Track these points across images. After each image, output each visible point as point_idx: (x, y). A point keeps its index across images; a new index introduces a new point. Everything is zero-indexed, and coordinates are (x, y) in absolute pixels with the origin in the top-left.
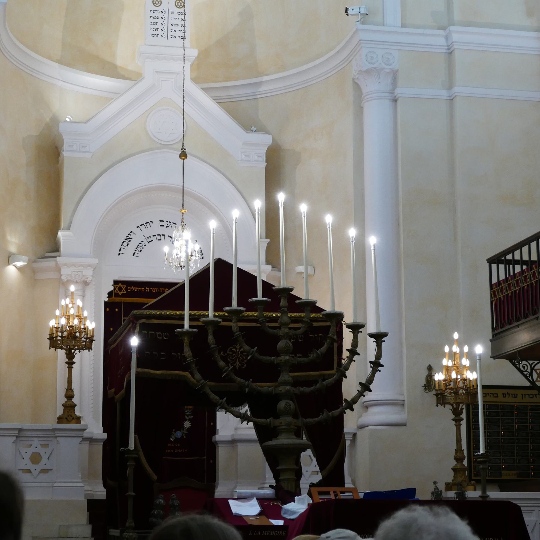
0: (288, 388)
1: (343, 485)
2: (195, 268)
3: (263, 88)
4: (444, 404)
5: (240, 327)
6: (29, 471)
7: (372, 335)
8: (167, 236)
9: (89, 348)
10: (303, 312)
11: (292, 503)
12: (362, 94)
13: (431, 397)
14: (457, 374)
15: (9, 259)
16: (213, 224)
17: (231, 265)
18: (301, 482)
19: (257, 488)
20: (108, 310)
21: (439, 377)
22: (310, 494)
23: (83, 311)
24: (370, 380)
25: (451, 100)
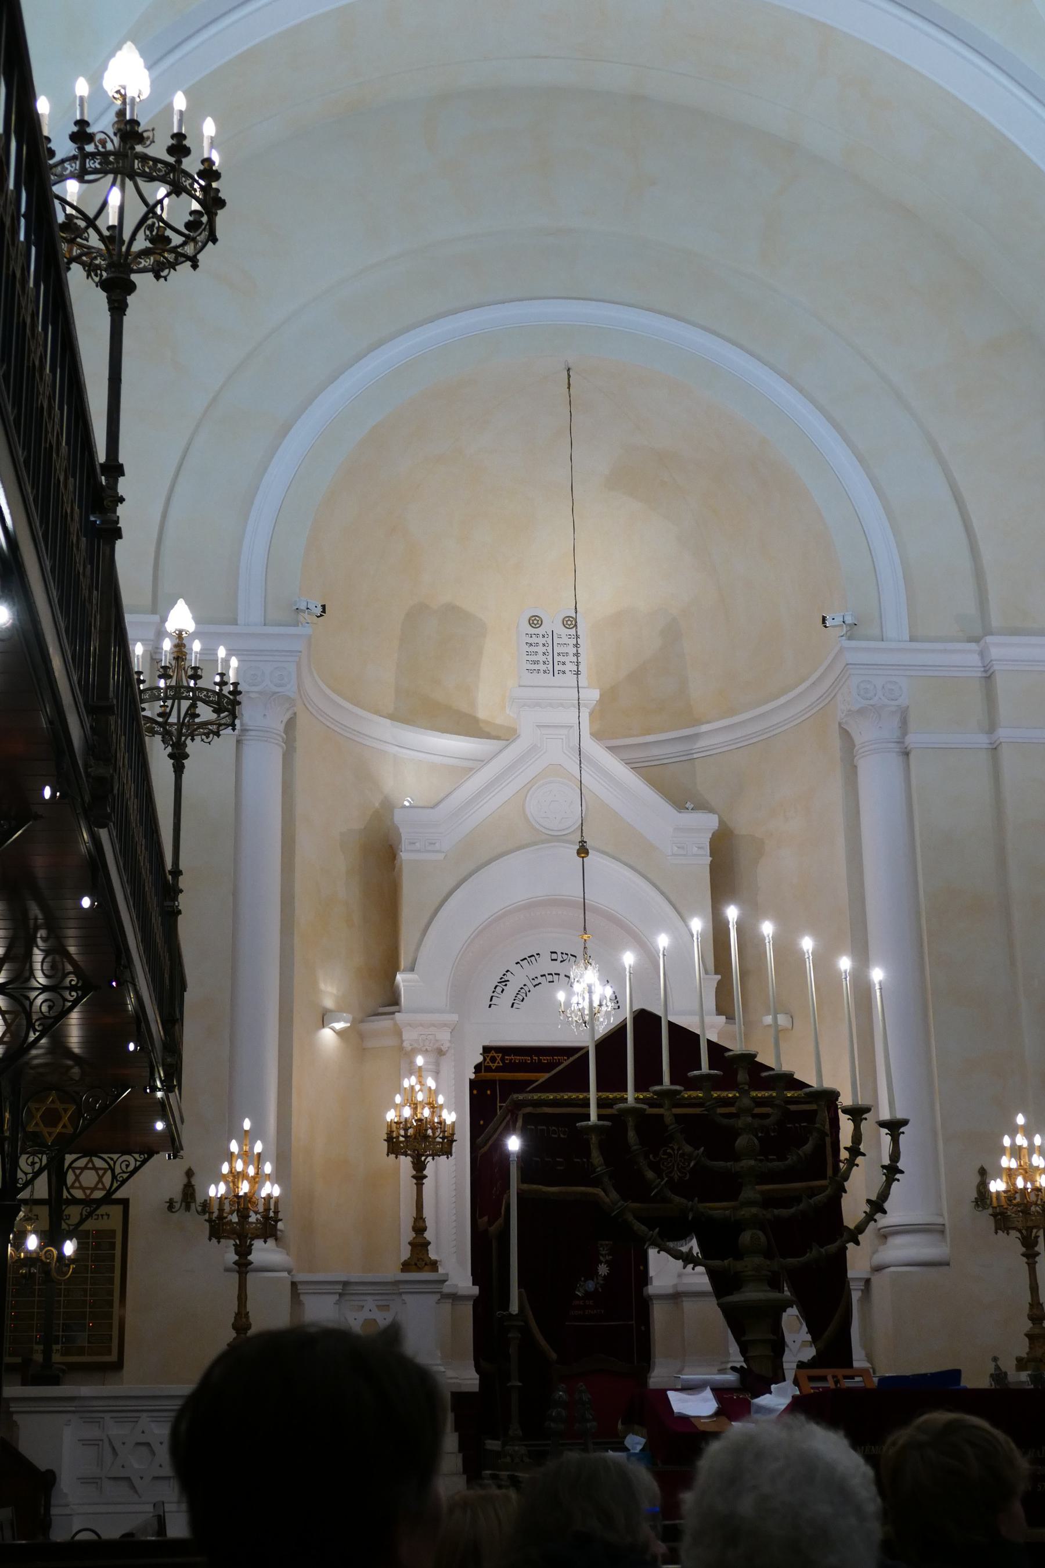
0: (754, 1210)
1: (850, 1364)
2: (602, 1028)
3: (701, 743)
4: (1007, 1229)
5: (676, 1116)
7: (883, 1124)
8: (562, 976)
9: (448, 1153)
10: (773, 1089)
11: (768, 1395)
12: (854, 746)
13: (985, 1220)
14: (1025, 1181)
15: (324, 1019)
16: (629, 958)
17: (658, 1019)
18: (784, 1359)
19: (715, 1370)
20: (475, 1092)
21: (997, 1186)
22: (796, 1382)
23: (437, 1097)
24: (884, 1195)
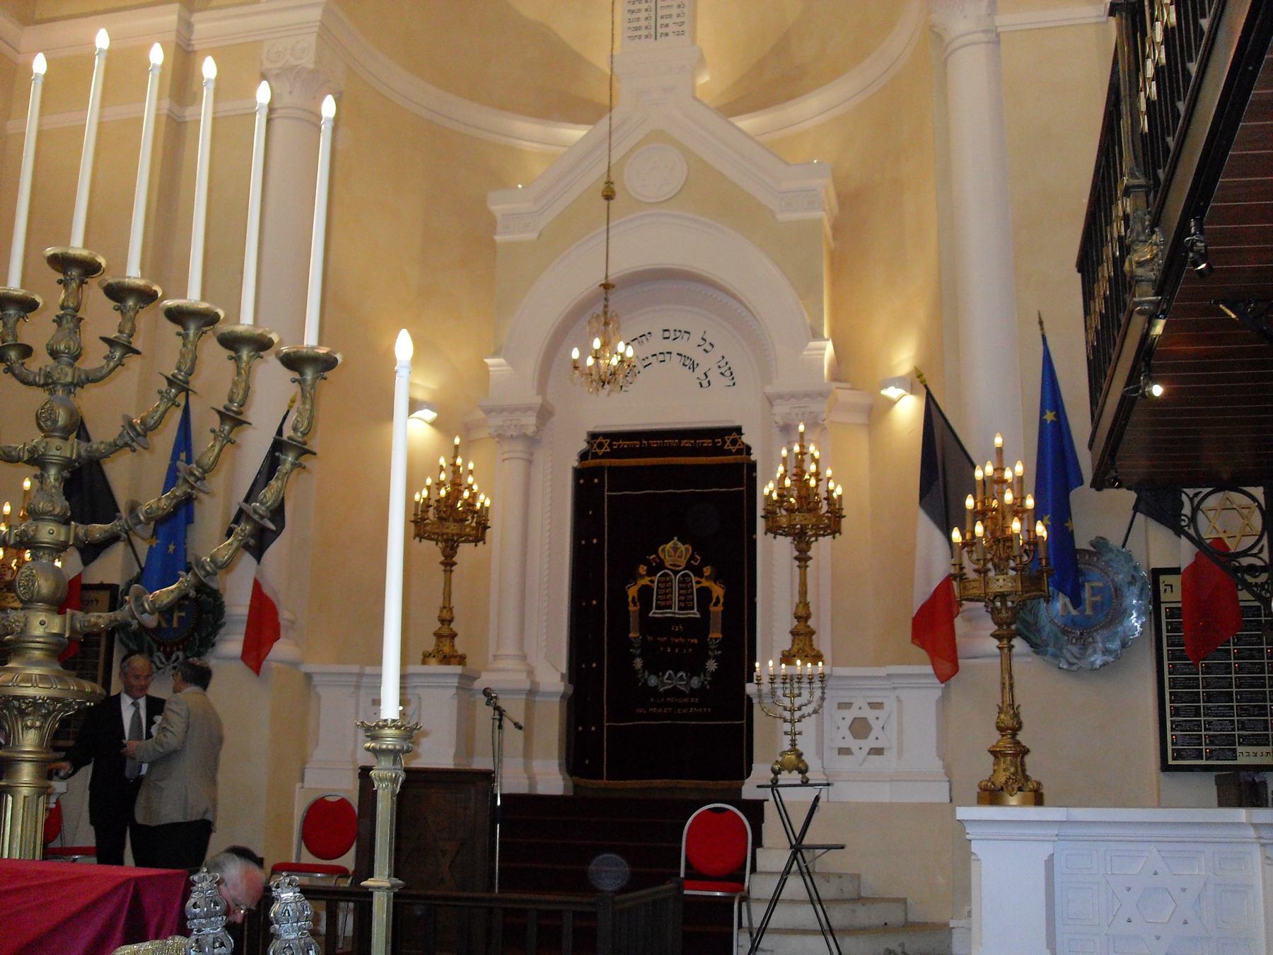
8: (674, 355)
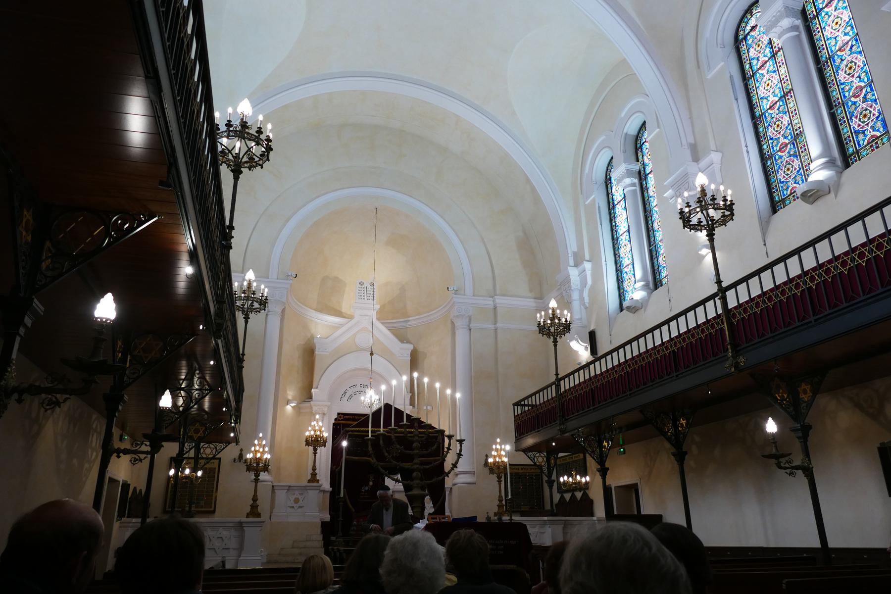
2: (375, 408)
3: (410, 323)
6: (293, 507)
13: (487, 470)
15: (288, 403)
21: (491, 460)
24: (457, 462)
25: (496, 329)
